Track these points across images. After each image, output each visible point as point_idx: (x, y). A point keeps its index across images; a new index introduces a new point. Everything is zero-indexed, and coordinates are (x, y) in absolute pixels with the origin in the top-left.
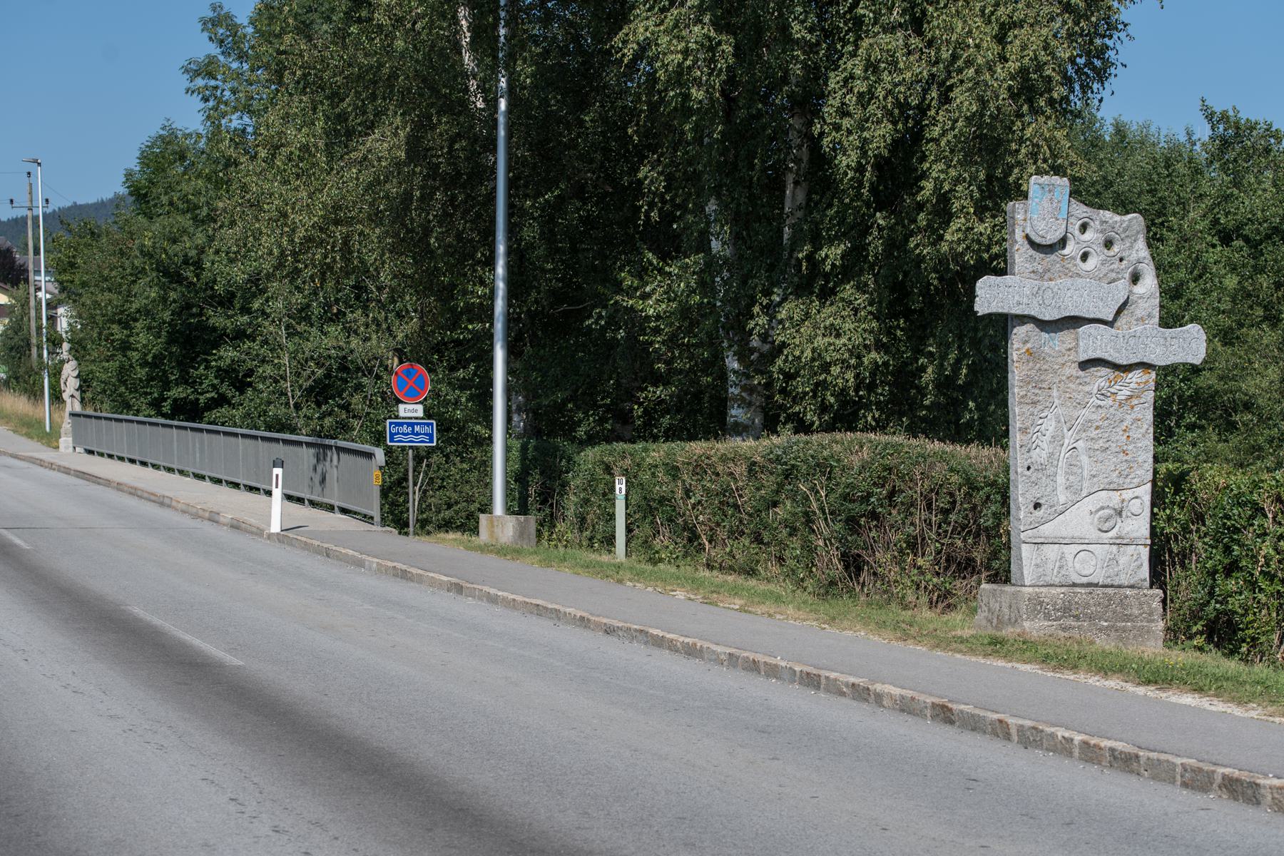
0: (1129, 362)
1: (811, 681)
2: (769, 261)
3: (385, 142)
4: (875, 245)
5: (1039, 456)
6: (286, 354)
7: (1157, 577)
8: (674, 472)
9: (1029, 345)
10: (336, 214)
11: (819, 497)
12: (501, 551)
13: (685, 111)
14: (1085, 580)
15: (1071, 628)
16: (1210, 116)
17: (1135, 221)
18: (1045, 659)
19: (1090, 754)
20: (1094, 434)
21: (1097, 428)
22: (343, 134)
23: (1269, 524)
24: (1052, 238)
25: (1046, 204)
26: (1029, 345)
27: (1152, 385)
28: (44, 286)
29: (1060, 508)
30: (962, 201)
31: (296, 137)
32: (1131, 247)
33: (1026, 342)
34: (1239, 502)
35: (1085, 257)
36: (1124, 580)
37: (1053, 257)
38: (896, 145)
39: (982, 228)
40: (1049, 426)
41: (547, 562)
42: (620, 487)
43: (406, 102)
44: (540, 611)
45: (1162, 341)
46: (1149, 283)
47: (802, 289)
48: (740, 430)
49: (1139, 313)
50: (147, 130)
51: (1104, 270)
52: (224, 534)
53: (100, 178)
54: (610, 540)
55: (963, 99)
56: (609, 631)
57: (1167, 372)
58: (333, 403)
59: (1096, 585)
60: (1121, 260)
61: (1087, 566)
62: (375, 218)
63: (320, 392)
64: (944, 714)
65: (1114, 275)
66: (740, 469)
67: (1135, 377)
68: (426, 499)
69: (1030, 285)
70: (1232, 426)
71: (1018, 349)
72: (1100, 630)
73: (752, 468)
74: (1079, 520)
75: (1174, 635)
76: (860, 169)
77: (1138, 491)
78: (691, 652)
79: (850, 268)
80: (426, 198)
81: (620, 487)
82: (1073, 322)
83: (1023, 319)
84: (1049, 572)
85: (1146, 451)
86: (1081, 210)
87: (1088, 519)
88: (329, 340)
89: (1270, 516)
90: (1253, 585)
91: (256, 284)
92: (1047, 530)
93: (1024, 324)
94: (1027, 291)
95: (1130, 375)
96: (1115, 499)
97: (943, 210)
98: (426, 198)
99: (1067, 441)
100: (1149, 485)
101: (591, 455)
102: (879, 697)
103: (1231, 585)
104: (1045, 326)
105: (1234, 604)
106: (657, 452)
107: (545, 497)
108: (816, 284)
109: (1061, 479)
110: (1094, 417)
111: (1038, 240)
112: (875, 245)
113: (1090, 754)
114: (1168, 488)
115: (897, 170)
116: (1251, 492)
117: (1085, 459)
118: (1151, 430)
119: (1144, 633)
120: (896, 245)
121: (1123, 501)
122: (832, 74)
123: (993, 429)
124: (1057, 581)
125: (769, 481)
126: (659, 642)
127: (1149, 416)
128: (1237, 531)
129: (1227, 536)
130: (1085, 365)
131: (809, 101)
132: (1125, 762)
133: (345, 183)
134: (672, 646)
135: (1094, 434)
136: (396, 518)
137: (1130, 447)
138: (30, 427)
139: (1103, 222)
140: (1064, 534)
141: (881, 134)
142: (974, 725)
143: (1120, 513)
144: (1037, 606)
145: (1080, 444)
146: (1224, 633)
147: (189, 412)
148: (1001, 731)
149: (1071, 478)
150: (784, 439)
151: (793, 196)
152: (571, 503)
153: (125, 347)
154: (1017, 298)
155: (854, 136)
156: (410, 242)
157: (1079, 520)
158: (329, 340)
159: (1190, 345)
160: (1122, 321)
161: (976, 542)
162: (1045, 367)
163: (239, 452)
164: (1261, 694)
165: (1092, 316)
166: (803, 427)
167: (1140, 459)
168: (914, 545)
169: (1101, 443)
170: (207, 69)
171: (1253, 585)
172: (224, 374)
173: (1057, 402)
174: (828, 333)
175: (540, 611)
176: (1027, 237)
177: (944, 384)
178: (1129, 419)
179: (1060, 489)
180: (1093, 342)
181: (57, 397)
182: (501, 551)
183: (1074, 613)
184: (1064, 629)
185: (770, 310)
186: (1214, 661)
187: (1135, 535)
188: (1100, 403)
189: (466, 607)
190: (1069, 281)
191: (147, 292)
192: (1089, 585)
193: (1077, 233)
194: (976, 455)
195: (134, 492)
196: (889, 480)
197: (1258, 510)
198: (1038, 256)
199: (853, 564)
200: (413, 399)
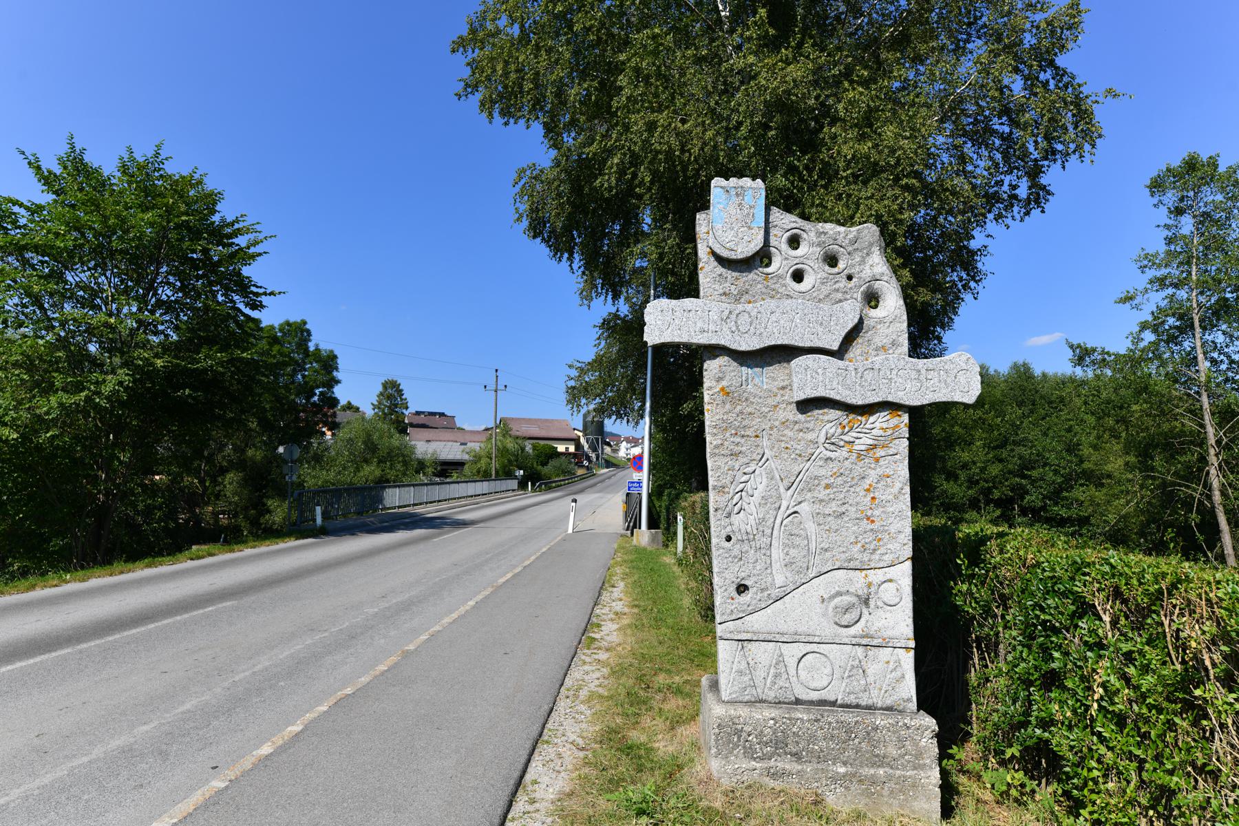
0: (867, 402)
7: (942, 686)
9: (724, 383)
14: (815, 696)
15: (783, 774)
16: (1071, 347)
20: (823, 494)
21: (827, 486)
23: (1105, 628)
24: (744, 250)
25: (733, 210)
26: (724, 383)
27: (905, 432)
29: (776, 593)
32: (863, 262)
33: (719, 380)
35: (798, 276)
36: (876, 698)
37: (751, 276)
40: (759, 484)
45: (914, 375)
46: (892, 304)
49: (879, 341)
51: (825, 290)
57: (918, 415)
59: (833, 703)
60: (850, 278)
61: (818, 676)
65: (839, 296)
67: (879, 421)
70: (1102, 485)
71: (710, 388)
72: (835, 779)
77: (892, 572)
82: (782, 353)
83: (715, 350)
84: (759, 681)
85: (900, 515)
86: (785, 221)
87: (819, 608)
89: (1107, 618)
92: (757, 622)
93: (715, 357)
94: (714, 316)
95: (872, 419)
99: (784, 504)
100: (909, 564)
109: (777, 553)
110: (822, 472)
111: (725, 254)
116: (1072, 579)
117: (811, 527)
118: (907, 489)
121: (869, 585)
124: (771, 695)
127: (903, 471)
128: (1056, 631)
130: (806, 405)
135: (823, 494)
137: (877, 513)
139: (819, 234)
140: (783, 628)
143: (866, 602)
144: (733, 737)
145: (805, 508)
149: (793, 552)
154: (699, 324)
160: (856, 351)
162: (749, 410)
165: (808, 344)
167: (893, 529)
169: (834, 506)
173: (768, 454)
176: (713, 253)
178: (873, 475)
179: (776, 566)
180: (810, 377)
183: (792, 748)
184: (774, 775)
187: (890, 633)
188: (829, 454)
190: (772, 304)
192: (822, 703)
193: (784, 246)
197: (1085, 609)
198: (730, 274)
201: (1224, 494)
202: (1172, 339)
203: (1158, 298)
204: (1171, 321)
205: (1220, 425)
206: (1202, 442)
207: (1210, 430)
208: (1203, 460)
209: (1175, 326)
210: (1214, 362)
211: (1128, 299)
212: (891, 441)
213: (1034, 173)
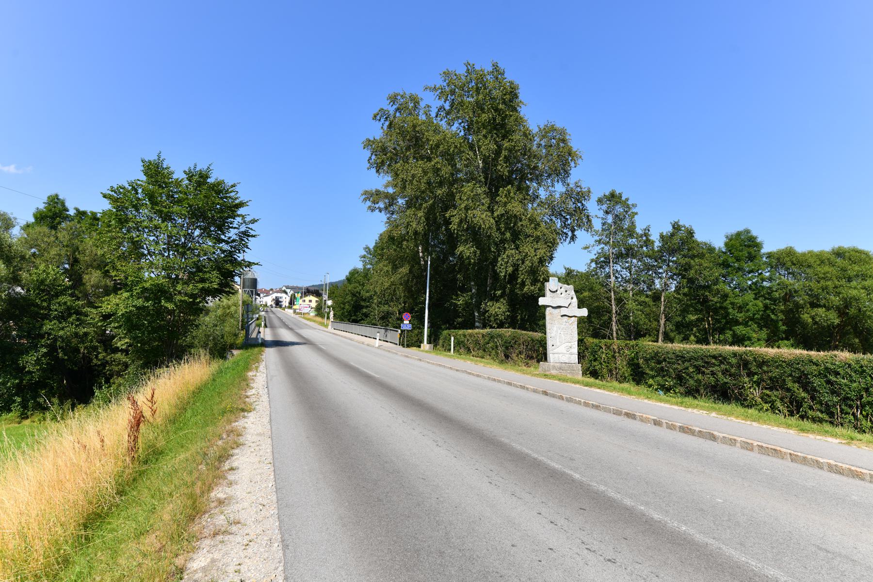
1: (509, 384)
2: (484, 294)
3: (404, 270)
4: (507, 290)
5: (553, 335)
6: (377, 311)
8: (465, 336)
10: (393, 284)
11: (500, 342)
12: (426, 352)
13: (470, 264)
17: (571, 287)
18: (559, 380)
19: (586, 404)
22: (395, 268)
28: (325, 297)
30: (528, 282)
31: (386, 269)
34: (596, 345)
38: (513, 271)
39: (532, 288)
40: (555, 329)
41: (437, 354)
42: (452, 338)
43: (409, 262)
44: (440, 365)
47: (492, 299)
48: (478, 328)
50: (350, 268)
52: (366, 347)
53: (339, 275)
54: (450, 350)
55: (527, 263)
56: (457, 370)
58: (386, 321)
61: (564, 359)
62: (401, 284)
63: (383, 318)
64: (545, 393)
66: (480, 336)
68: (411, 341)
69: (550, 299)
73: (483, 336)
74: (562, 349)
75: (584, 373)
76: (505, 276)
78: (478, 376)
79: (502, 296)
80: (412, 281)
81: (452, 338)
82: (560, 307)
86: (560, 284)
88: (386, 308)
90: (601, 364)
91: (371, 297)
92: (555, 351)
96: (570, 345)
97: (523, 284)
98: (412, 281)
101: (445, 332)
102: (527, 389)
103: (596, 364)
104: (553, 307)
105: (597, 368)
106: (461, 332)
107: (435, 341)
108: (495, 299)
112: (507, 290)
113: (586, 404)
114: (580, 342)
115: (513, 277)
119: (578, 374)
120: (512, 291)
122: (81, 333)
123: (543, 329)
125: (487, 339)
126: (470, 373)
129: (594, 353)
131: (495, 261)
132: (597, 407)
133: (396, 278)
134: (473, 375)
136: (403, 345)
138: (322, 324)
141: (510, 269)
142: (553, 396)
144: (554, 367)
146: (595, 374)
147: (355, 321)
148: (561, 398)
150: (488, 330)
151: (489, 281)
152: (441, 342)
153: (343, 309)
155: (503, 269)
156: (408, 289)
157: (562, 349)
158: (386, 308)
159: (584, 312)
161: (538, 353)
163: (368, 330)
164: (767, 410)
166: (491, 327)
168: (520, 353)
170: (364, 257)
171: (601, 364)
172: (363, 314)
174: (498, 308)
175: (440, 365)
177: (522, 319)
181: (328, 318)
182: (426, 352)
185: (486, 304)
186: (592, 380)
189: (422, 364)
191: (349, 298)
194: (537, 335)
195: (345, 338)
196: (515, 339)
197: (601, 348)
199: (507, 357)
200: (407, 319)
201: (617, 333)
202: (602, 267)
203: (598, 249)
204: (602, 259)
205: (617, 305)
206: (610, 312)
207: (614, 307)
208: (610, 319)
209: (603, 261)
210: (616, 278)
211: (586, 248)
212: (574, 321)
213: (573, 231)
